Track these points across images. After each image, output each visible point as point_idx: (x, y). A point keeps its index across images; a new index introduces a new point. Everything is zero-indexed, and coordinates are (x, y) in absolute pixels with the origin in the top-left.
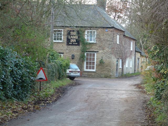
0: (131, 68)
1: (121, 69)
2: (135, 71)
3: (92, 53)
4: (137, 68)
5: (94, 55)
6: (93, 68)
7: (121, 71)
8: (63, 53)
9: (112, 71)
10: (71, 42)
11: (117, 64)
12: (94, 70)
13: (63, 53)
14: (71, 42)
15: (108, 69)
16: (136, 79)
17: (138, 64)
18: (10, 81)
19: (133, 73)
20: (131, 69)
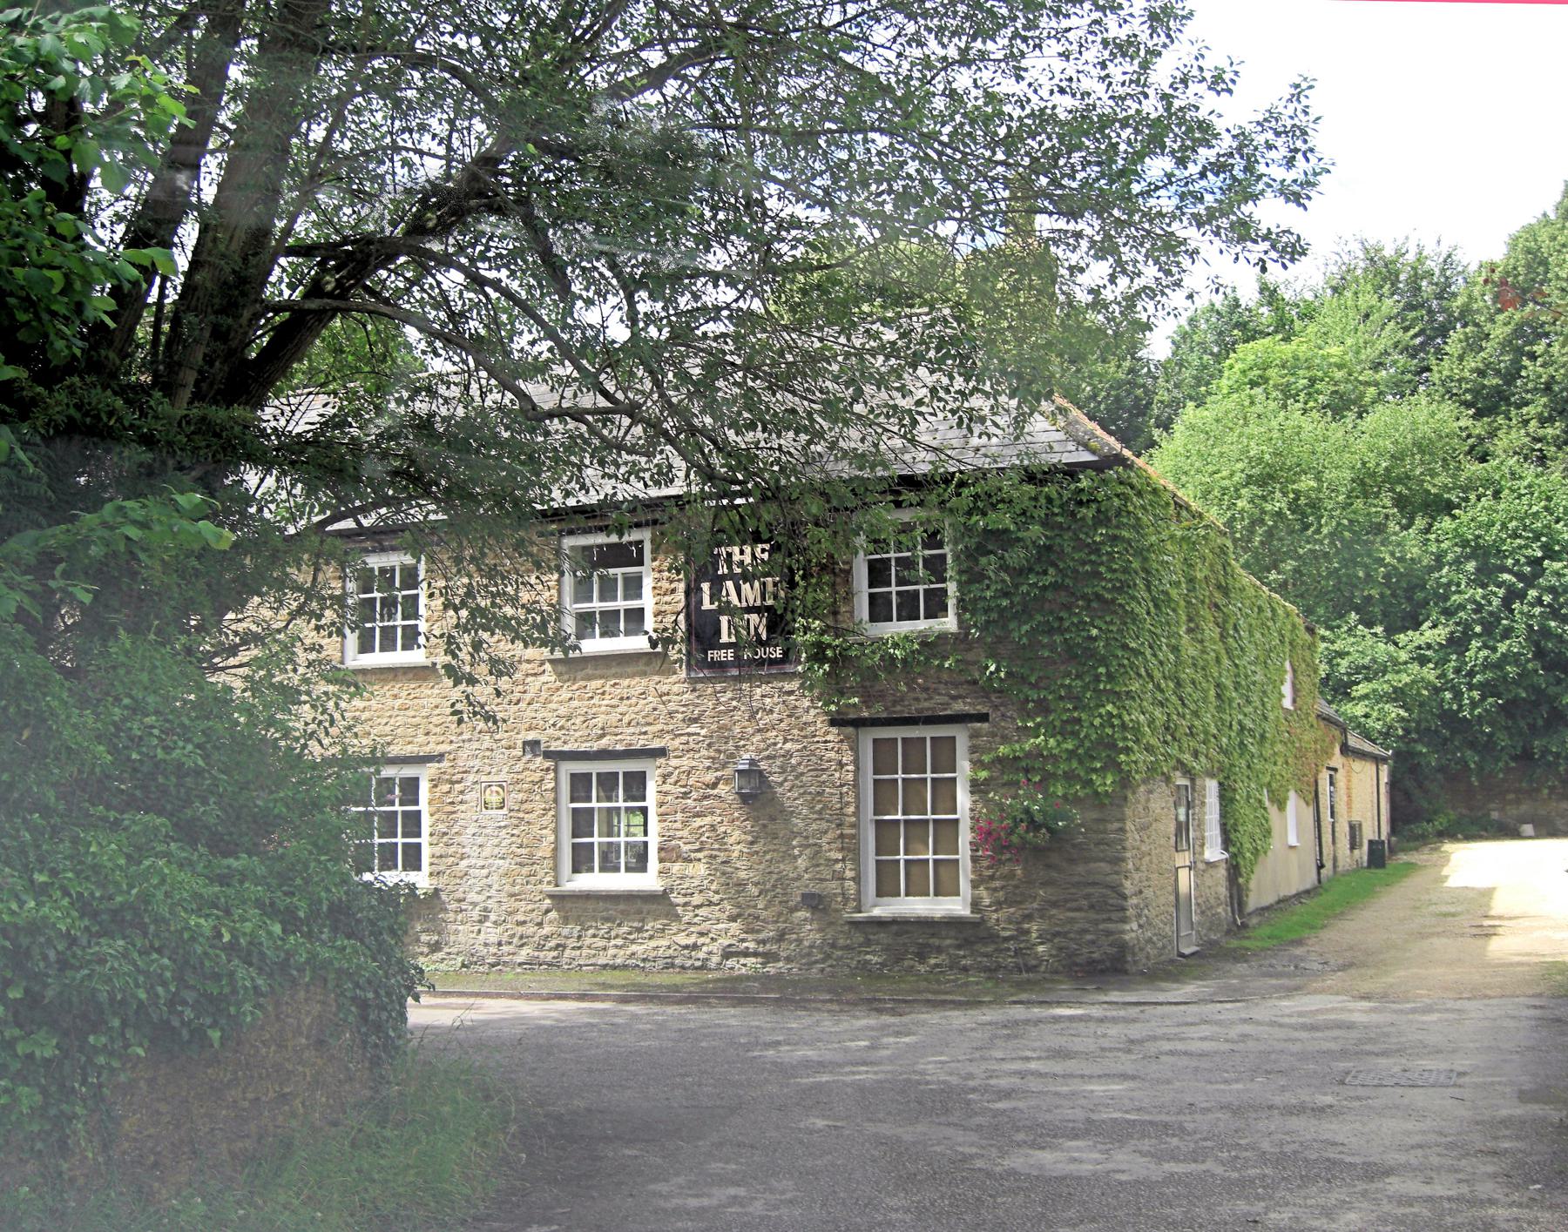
0: (1292, 847)
1: (1222, 872)
2: (1321, 867)
3: (928, 732)
4: (1327, 838)
5: (945, 748)
6: (946, 888)
7: (1223, 891)
8: (662, 752)
9: (1134, 901)
10: (728, 646)
11: (1179, 824)
12: (956, 906)
13: (662, 752)
14: (724, 639)
15: (1094, 884)
16: (1442, 1078)
17: (1332, 815)
18: (129, 1065)
19: (1308, 886)
20: (1293, 855)
